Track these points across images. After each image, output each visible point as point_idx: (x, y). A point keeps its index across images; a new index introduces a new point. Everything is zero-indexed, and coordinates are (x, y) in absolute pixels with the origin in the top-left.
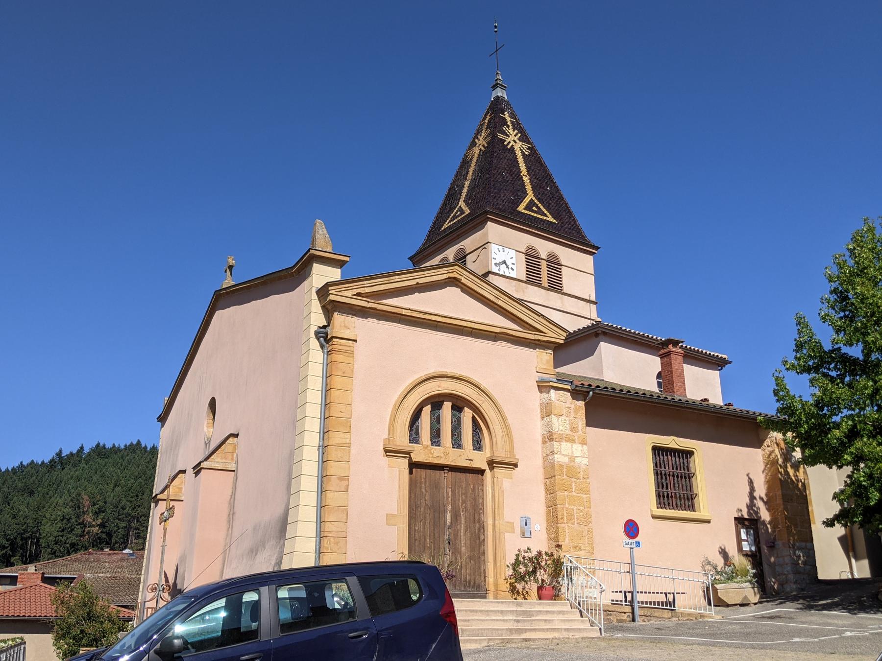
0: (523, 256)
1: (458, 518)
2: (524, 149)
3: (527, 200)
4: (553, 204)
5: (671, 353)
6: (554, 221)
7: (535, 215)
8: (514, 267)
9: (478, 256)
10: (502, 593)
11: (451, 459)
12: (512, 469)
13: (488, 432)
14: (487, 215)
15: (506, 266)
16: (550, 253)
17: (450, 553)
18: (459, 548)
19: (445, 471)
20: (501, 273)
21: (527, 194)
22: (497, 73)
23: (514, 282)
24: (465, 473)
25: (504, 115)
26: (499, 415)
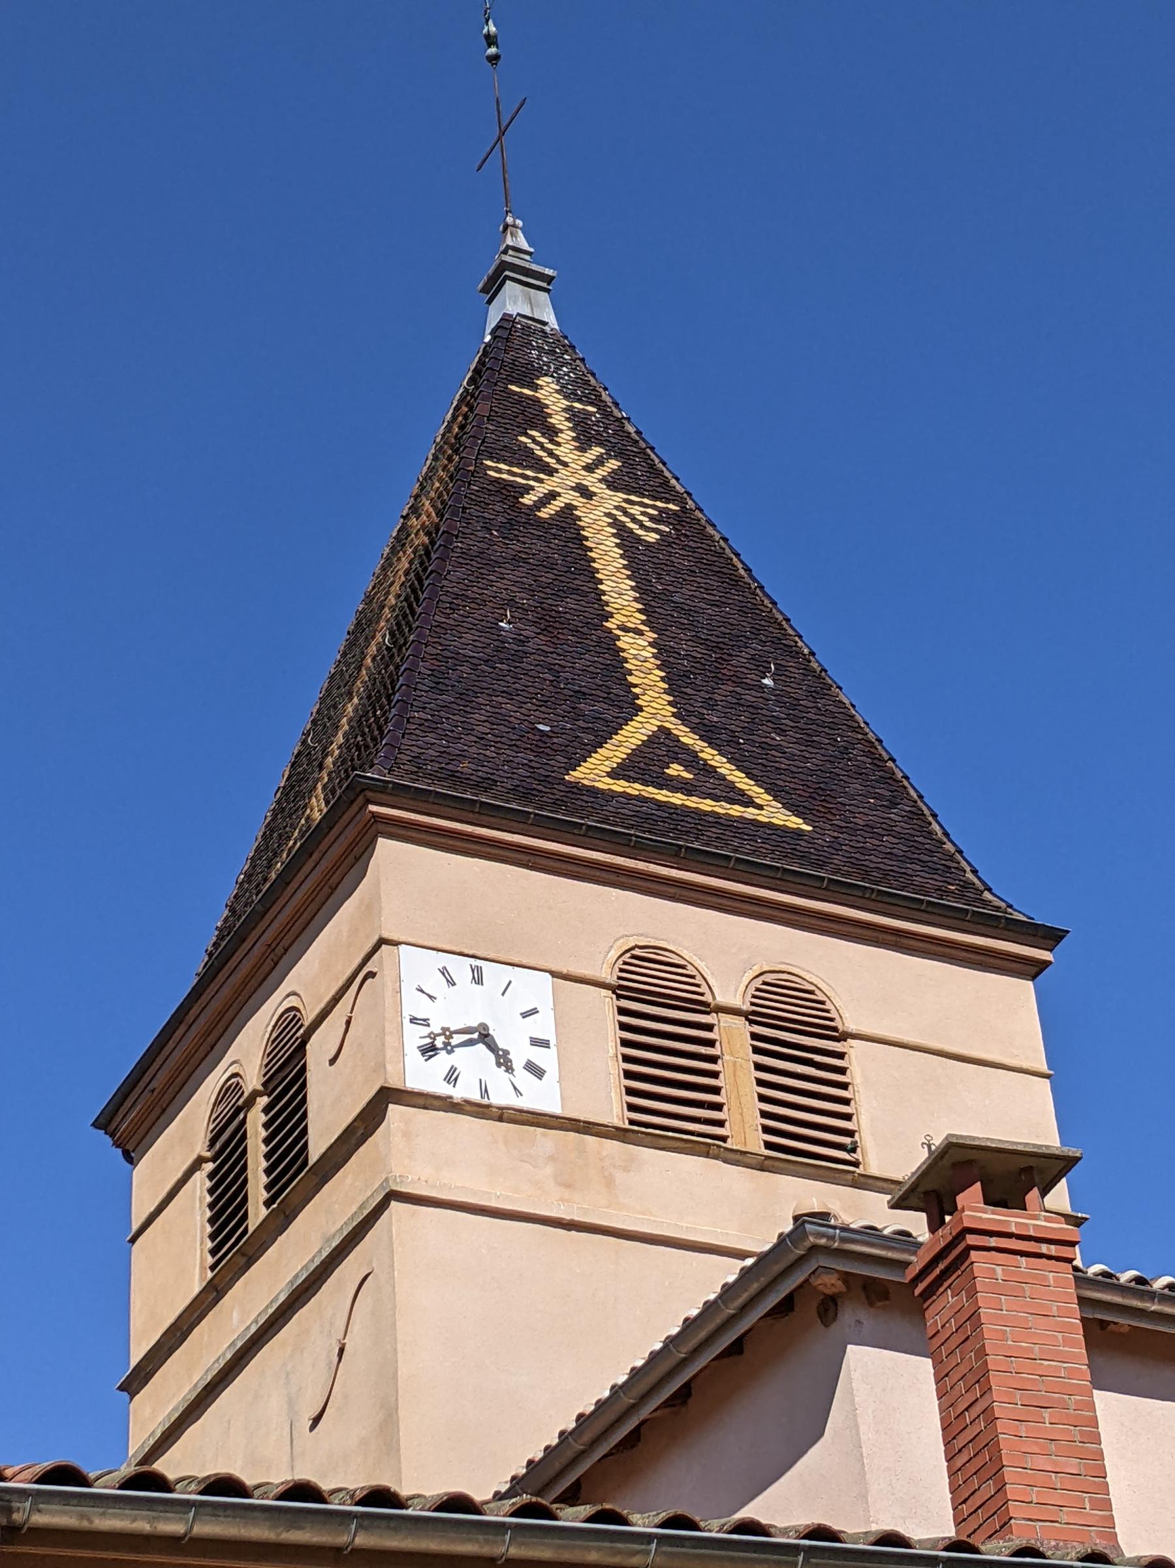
0: (606, 1002)
2: (634, 519)
3: (633, 734)
4: (794, 749)
5: (971, 1239)
6: (795, 822)
7: (677, 799)
8: (546, 1058)
9: (348, 1023)
14: (369, 801)
15: (491, 1057)
16: (769, 978)
20: (465, 1091)
21: (640, 709)
22: (506, 227)
23: (547, 1140)
25: (536, 388)
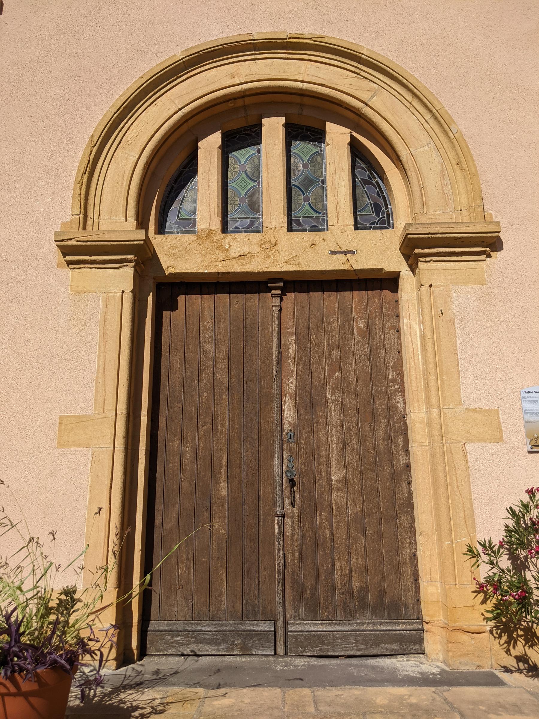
1: (320, 412)
10: (465, 637)
11: (283, 257)
12: (483, 257)
13: (403, 178)
17: (296, 511)
18: (326, 491)
19: (273, 292)
24: (337, 291)
26: (428, 117)
